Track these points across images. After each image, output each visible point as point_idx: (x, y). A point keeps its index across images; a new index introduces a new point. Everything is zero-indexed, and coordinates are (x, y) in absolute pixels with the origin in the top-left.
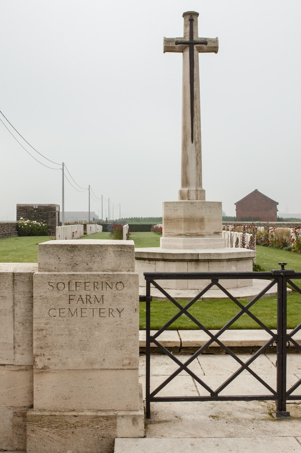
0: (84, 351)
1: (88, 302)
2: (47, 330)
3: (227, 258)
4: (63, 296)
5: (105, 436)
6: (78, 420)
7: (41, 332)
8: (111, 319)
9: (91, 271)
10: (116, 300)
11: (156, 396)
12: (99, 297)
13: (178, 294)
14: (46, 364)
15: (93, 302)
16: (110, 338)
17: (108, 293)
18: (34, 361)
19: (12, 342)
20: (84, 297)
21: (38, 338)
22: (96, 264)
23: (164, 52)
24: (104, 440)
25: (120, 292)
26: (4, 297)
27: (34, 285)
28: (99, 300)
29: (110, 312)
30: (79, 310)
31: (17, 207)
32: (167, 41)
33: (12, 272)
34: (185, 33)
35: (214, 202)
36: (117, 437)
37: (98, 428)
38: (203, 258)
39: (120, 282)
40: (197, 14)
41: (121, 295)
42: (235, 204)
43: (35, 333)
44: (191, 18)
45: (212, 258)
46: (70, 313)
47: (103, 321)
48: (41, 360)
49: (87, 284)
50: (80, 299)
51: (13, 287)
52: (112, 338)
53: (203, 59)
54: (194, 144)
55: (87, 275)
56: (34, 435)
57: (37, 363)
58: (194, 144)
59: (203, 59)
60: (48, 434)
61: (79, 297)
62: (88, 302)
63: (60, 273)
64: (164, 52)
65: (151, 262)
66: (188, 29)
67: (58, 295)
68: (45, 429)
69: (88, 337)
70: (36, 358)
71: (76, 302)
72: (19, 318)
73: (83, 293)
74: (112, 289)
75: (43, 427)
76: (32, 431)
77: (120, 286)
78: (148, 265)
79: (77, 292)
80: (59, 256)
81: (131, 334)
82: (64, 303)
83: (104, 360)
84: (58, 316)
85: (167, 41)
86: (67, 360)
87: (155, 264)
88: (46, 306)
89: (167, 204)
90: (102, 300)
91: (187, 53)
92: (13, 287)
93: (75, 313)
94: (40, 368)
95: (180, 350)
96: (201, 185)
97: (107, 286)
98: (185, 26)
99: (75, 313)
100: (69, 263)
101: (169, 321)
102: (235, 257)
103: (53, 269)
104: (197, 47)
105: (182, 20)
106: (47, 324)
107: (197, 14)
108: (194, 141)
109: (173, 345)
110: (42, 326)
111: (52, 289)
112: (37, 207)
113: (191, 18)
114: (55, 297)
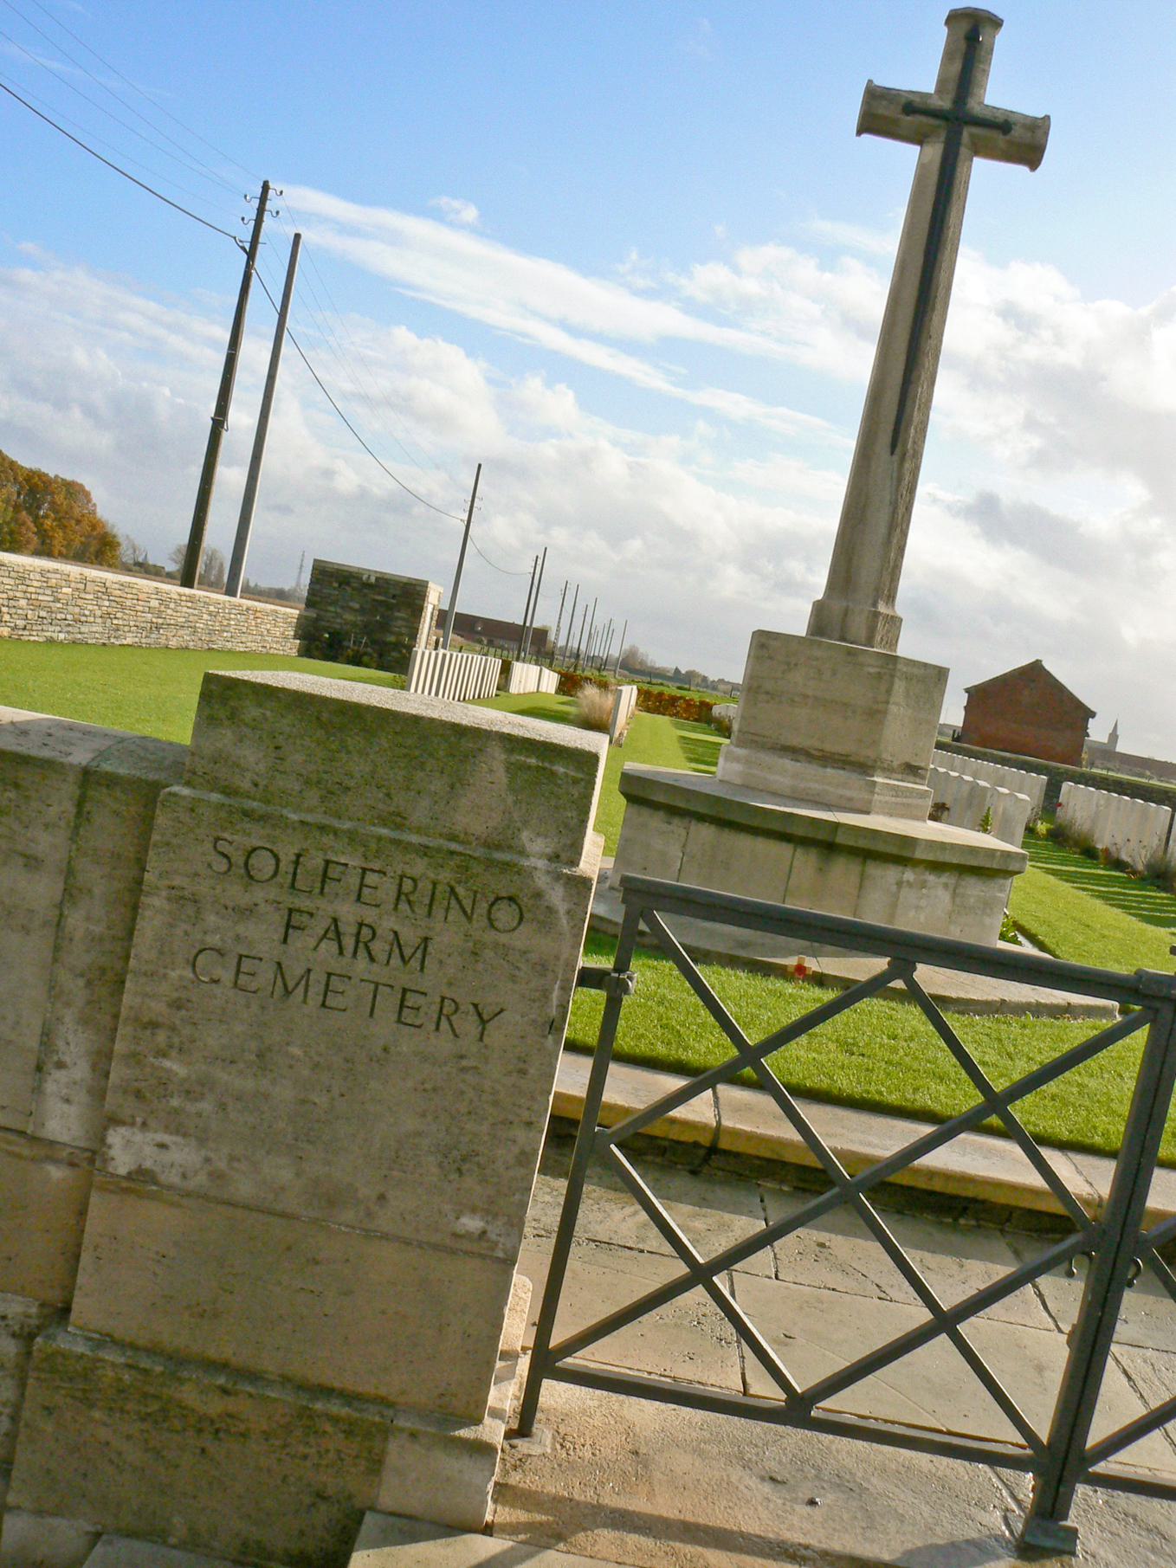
0: (310, 1147)
1: (362, 952)
2: (173, 1029)
3: (930, 857)
4: (263, 907)
5: (330, 1491)
6: (231, 1408)
7: (148, 1032)
8: (443, 1044)
9: (398, 827)
10: (480, 967)
11: (569, 1361)
12: (410, 937)
13: (745, 945)
14: (148, 1164)
15: (381, 956)
16: (423, 1115)
17: (448, 934)
18: (103, 1140)
19: (33, 1043)
20: (348, 929)
21: (134, 1055)
22: (425, 803)
23: (859, 133)
24: (323, 1507)
25: (503, 938)
26: (32, 862)
27: (155, 837)
28: (408, 952)
29: (445, 1013)
30: (318, 977)
31: (314, 568)
32: (874, 95)
33: (84, 763)
34: (941, 82)
35: (925, 665)
36: (372, 1509)
37: (305, 1457)
38: (851, 843)
39: (511, 899)
40: (997, 23)
41: (504, 951)
42: (967, 690)
43: (124, 1030)
44: (971, 36)
45: (881, 847)
46: (279, 982)
47: (407, 1044)
48: (128, 1143)
49: (371, 879)
50: (331, 935)
51: (77, 827)
52: (430, 1118)
53: (986, 177)
54: (896, 458)
55: (379, 839)
56: (49, 1428)
57: (112, 1153)
58: (896, 458)
59: (986, 177)
60: (103, 1434)
61: (328, 922)
62: (362, 952)
63: (270, 809)
64: (859, 133)
65: (676, 821)
66: (957, 66)
67: (245, 900)
68: (97, 1415)
69: (336, 1091)
70: (111, 1132)
71: (312, 942)
72: (80, 956)
73: (348, 913)
74: (469, 919)
75: (92, 1406)
76: (47, 1408)
77: (505, 914)
78: (665, 827)
79: (321, 903)
80: (280, 740)
81: (511, 1117)
82: (262, 935)
83: (382, 1198)
84: (230, 984)
85: (874, 95)
86: (236, 1165)
87: (687, 829)
88: (186, 933)
89: (764, 643)
90: (419, 955)
91: (935, 151)
92: (77, 827)
93: (301, 988)
94: (122, 1171)
95: (706, 1159)
96: (894, 598)
97: (453, 902)
98: (948, 56)
99: (301, 988)
100: (314, 777)
101: (614, 1396)
102: (955, 861)
103: (246, 785)
104: (972, 135)
105: (939, 36)
106: (177, 1005)
107: (997, 23)
108: (898, 450)
109: (687, 1137)
110: (158, 1008)
111: (224, 868)
112: (373, 580)
113: (971, 36)
114: (230, 904)
